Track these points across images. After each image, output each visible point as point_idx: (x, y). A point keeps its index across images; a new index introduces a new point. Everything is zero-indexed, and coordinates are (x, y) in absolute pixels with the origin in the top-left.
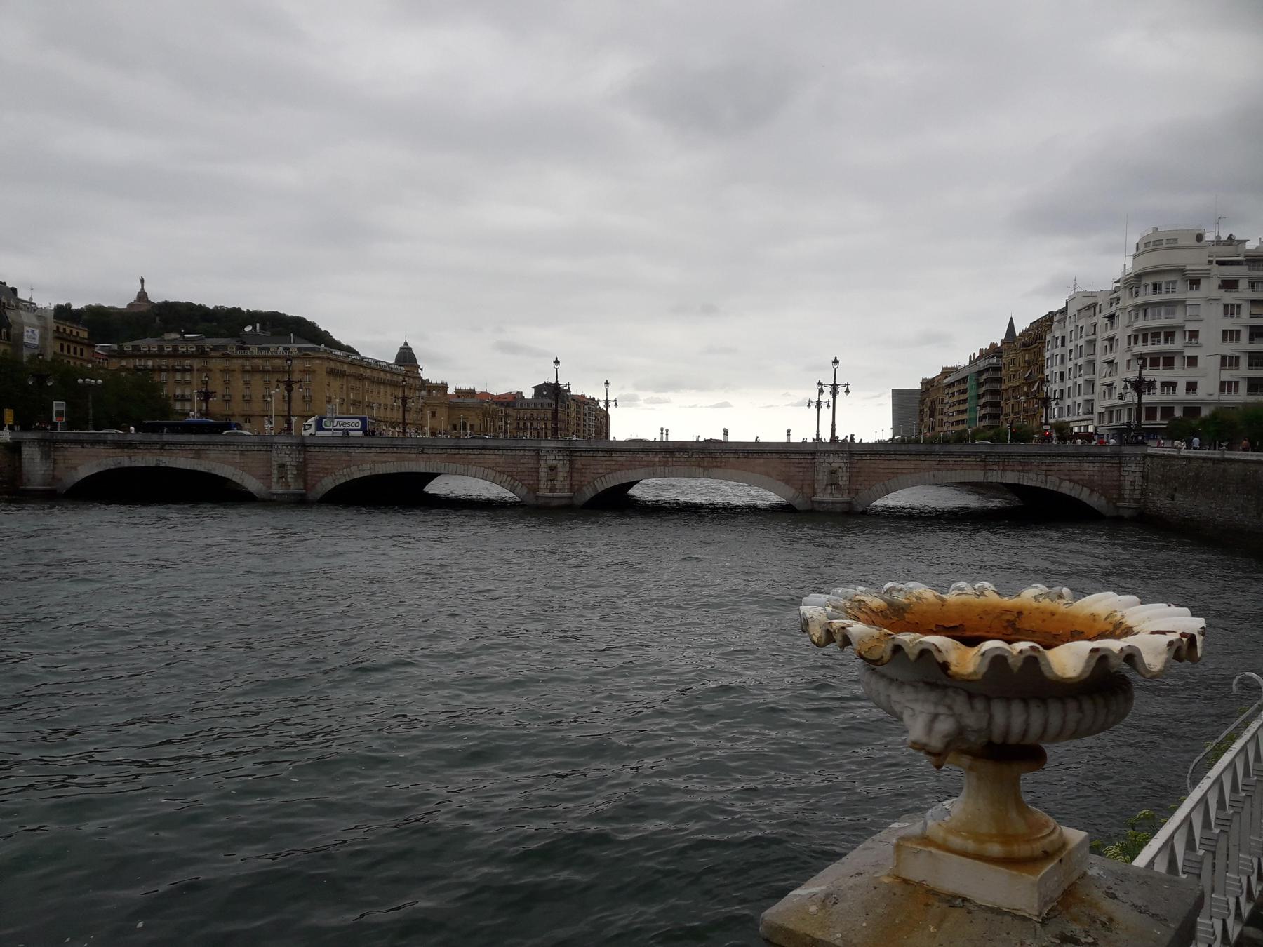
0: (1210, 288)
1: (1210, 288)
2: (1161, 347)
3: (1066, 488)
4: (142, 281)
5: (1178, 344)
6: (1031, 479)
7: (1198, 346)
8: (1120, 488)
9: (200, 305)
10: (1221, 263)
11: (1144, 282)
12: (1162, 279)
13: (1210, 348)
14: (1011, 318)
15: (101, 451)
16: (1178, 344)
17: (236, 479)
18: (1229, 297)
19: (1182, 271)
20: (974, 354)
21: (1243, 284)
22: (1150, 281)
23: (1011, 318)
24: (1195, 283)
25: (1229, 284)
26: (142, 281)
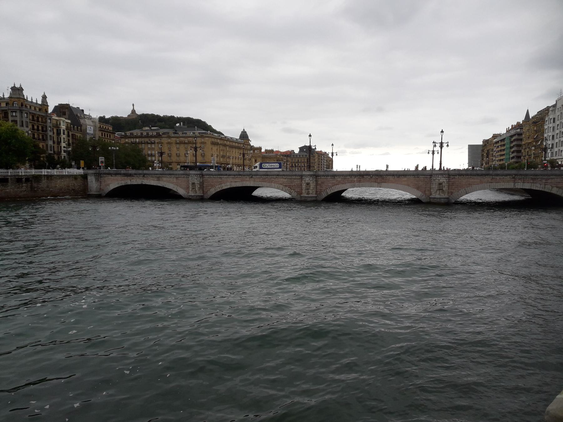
4: (133, 105)
9: (157, 115)
14: (528, 110)
20: (509, 128)
23: (528, 110)
26: (133, 105)
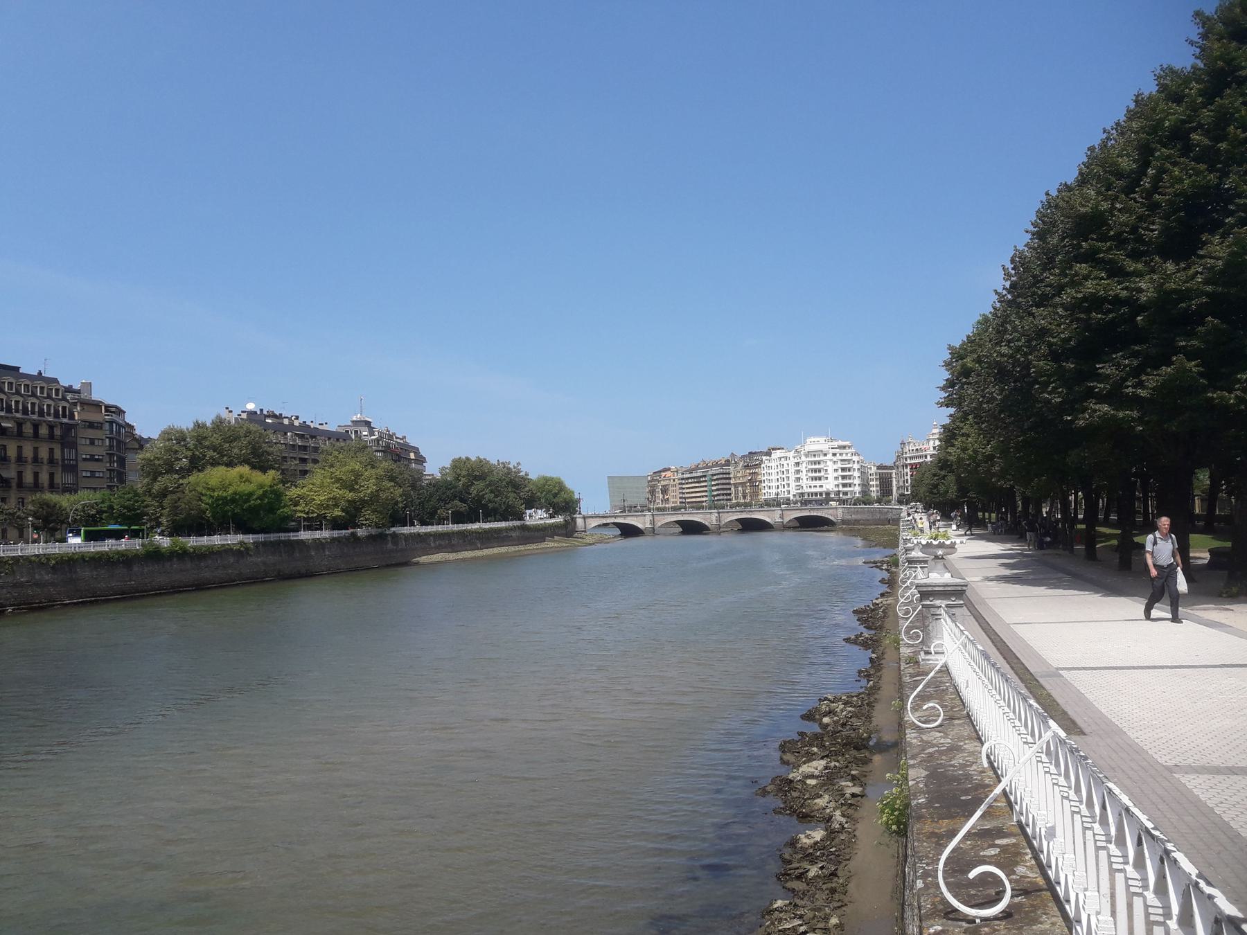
0: (830, 456)
1: (830, 456)
2: (817, 466)
3: (826, 516)
5: (822, 466)
6: (744, 516)
7: (828, 474)
8: (837, 515)
10: (832, 448)
11: (810, 453)
12: (816, 453)
13: (831, 475)
15: (598, 519)
16: (822, 466)
17: (635, 524)
18: (835, 459)
19: (822, 451)
21: (838, 455)
22: (813, 454)
24: (825, 455)
25: (834, 455)
